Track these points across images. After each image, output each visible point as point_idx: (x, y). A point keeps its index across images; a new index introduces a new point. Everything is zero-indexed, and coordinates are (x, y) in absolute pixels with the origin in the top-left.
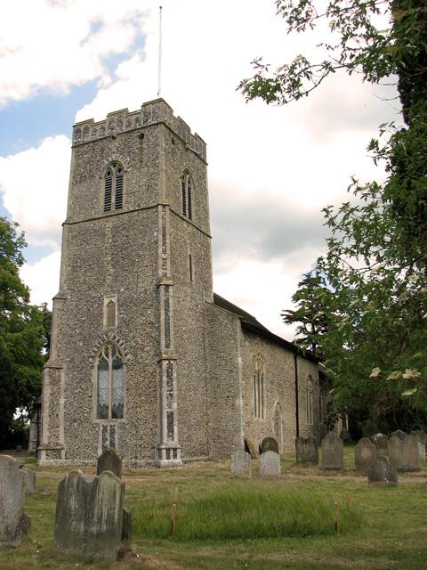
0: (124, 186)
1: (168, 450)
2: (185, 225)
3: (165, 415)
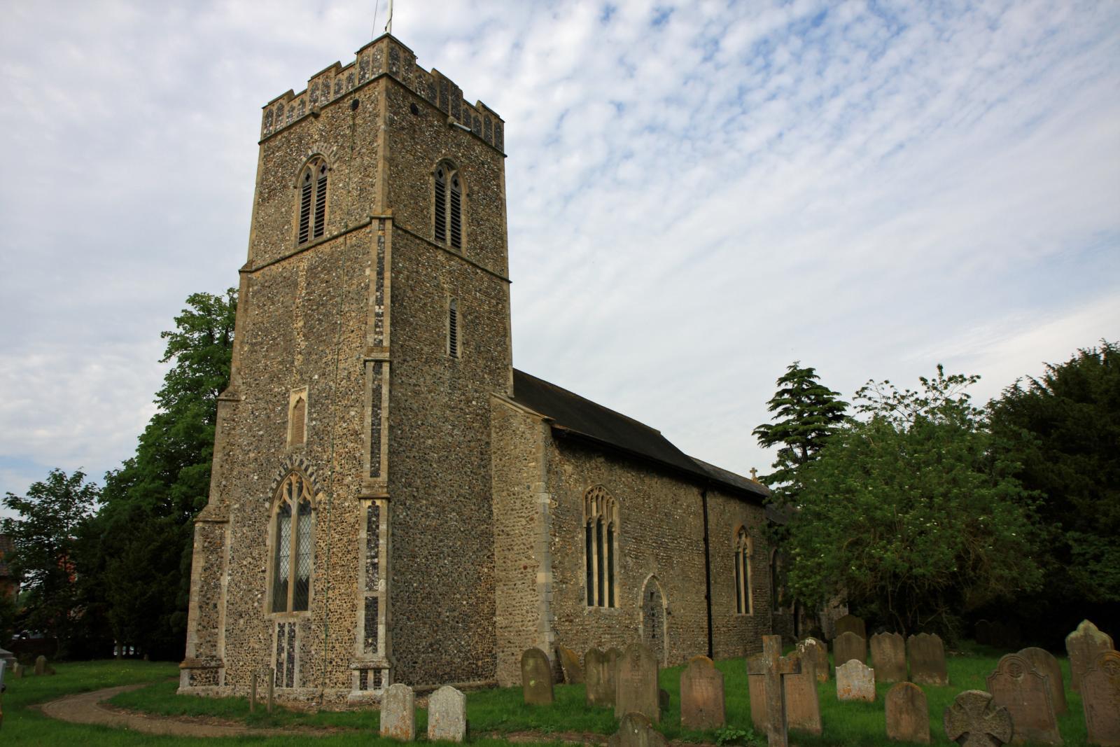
0: (327, 195)
1: (364, 671)
2: (441, 257)
3: (362, 604)
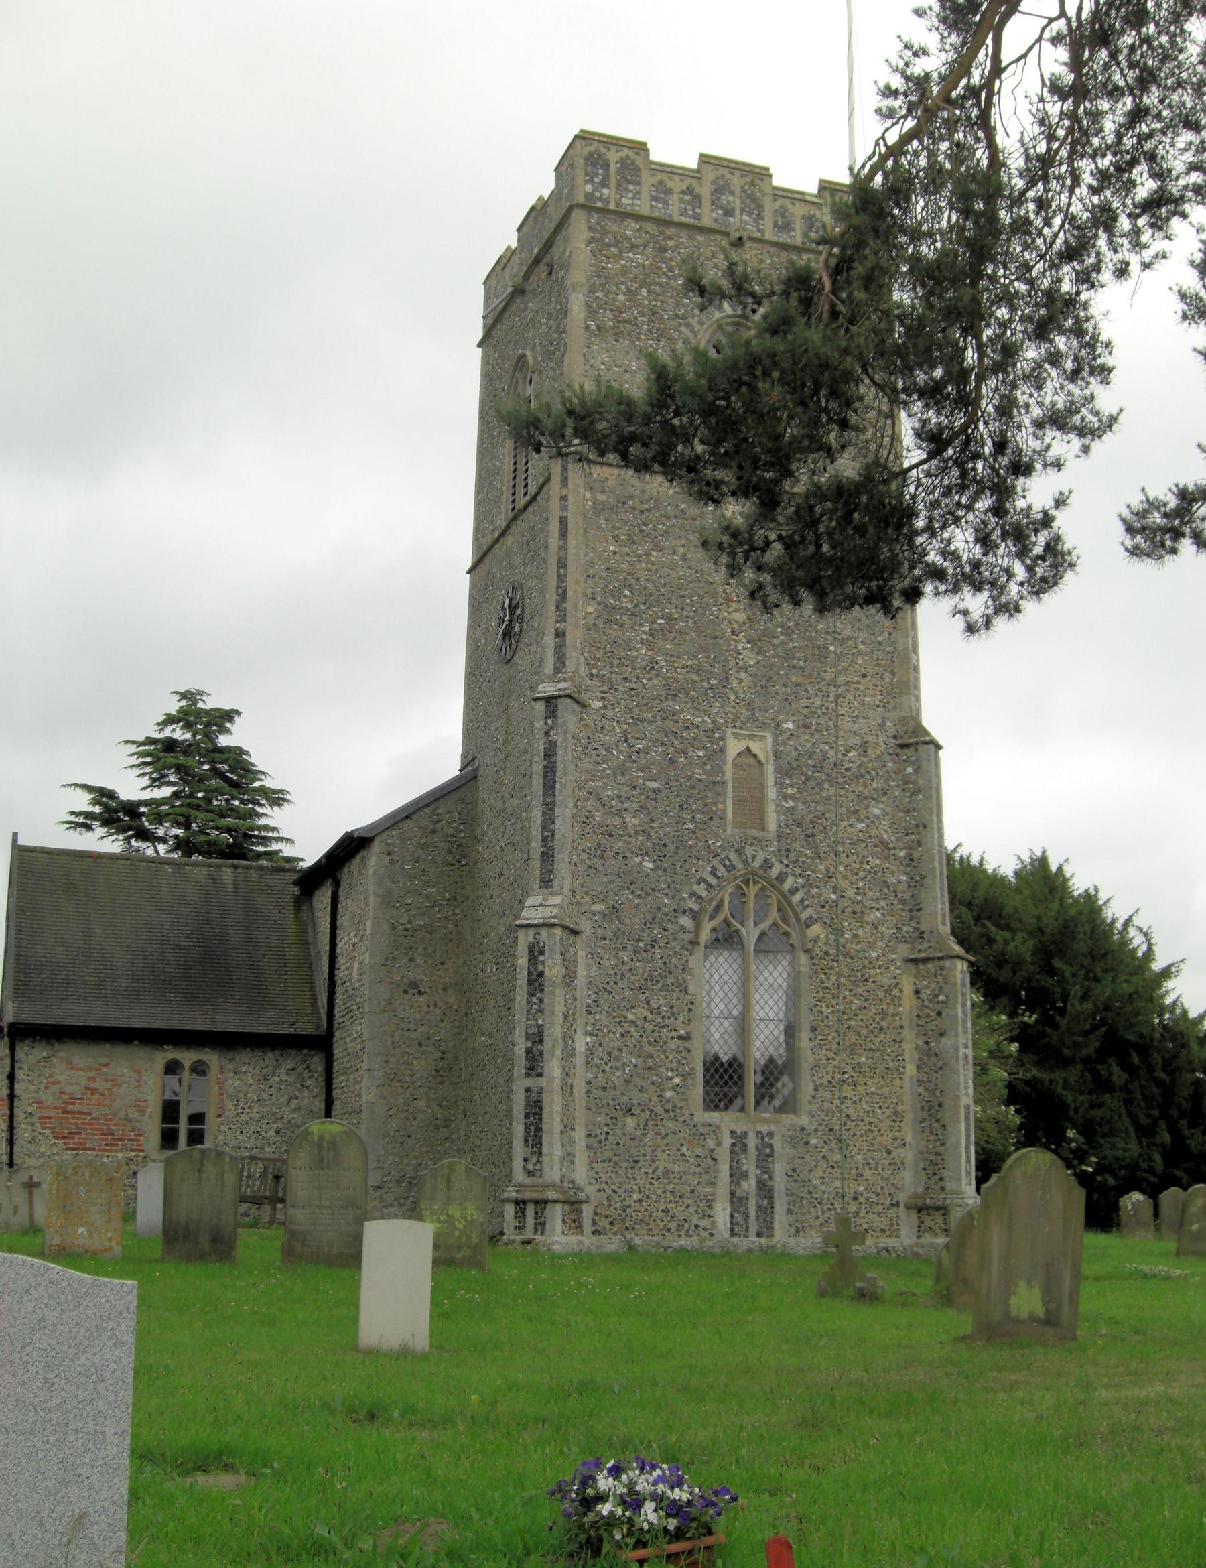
1: (520, 1204)
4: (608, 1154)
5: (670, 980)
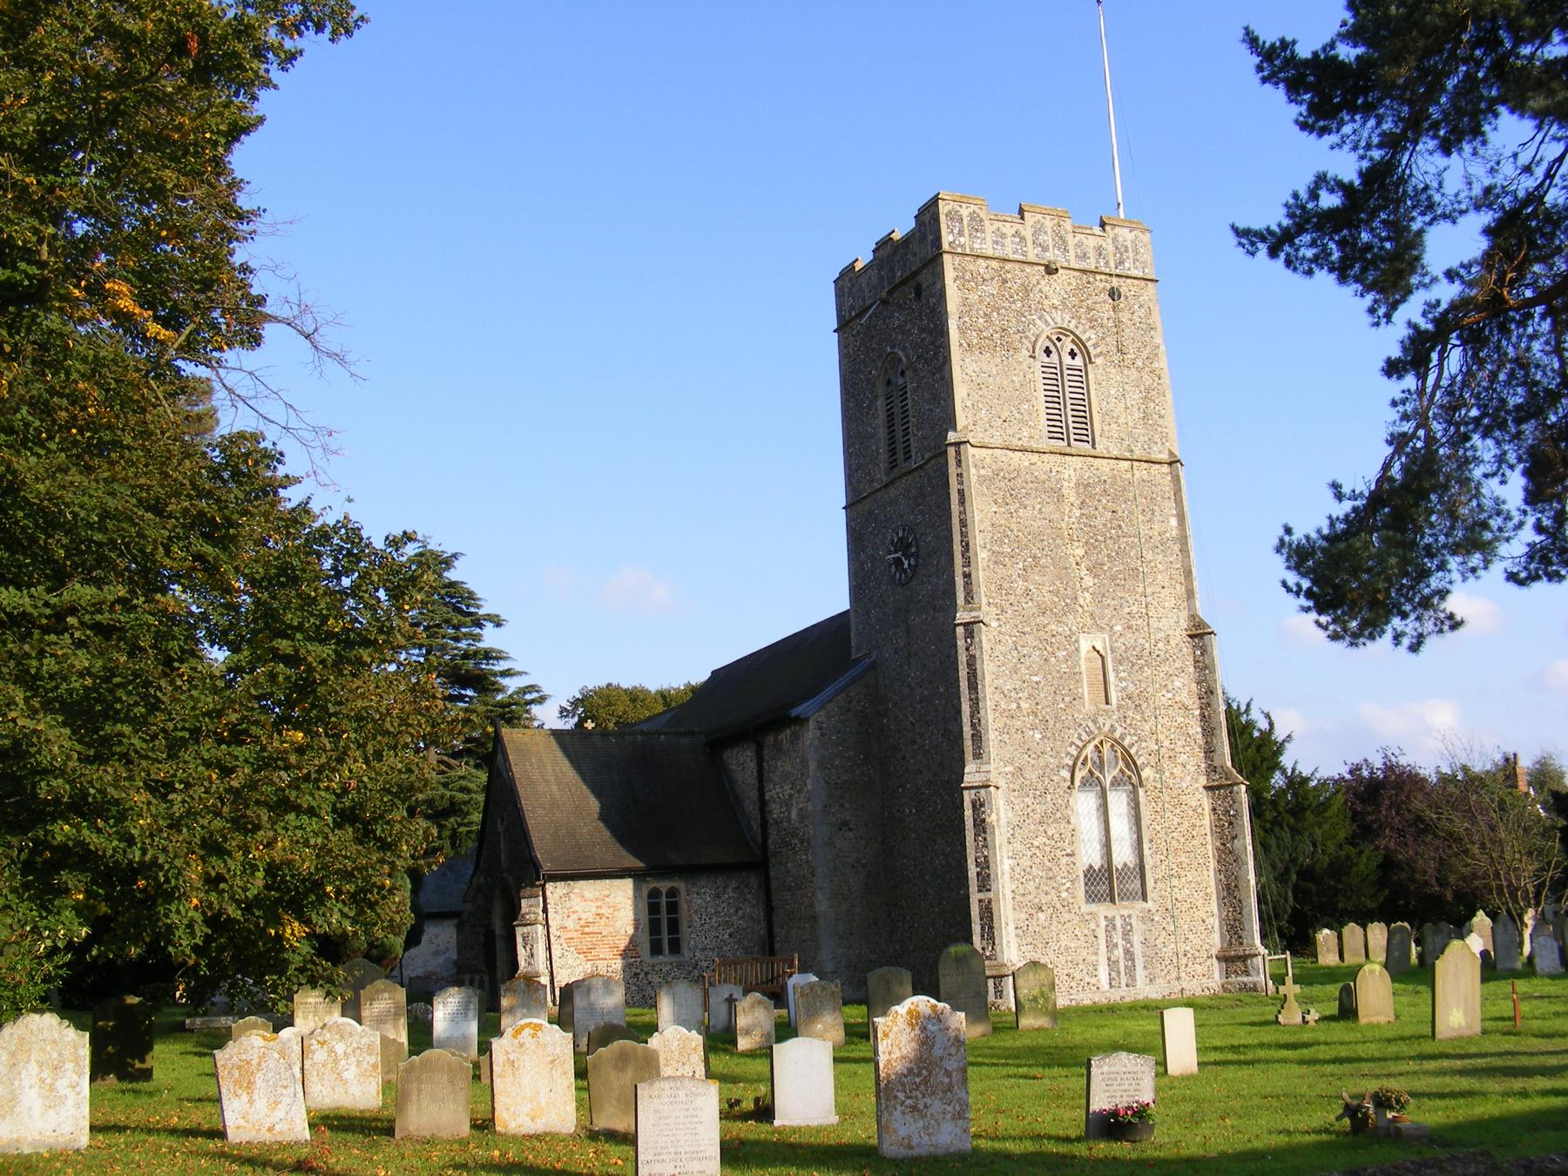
4: (1029, 940)
5: (1058, 815)
